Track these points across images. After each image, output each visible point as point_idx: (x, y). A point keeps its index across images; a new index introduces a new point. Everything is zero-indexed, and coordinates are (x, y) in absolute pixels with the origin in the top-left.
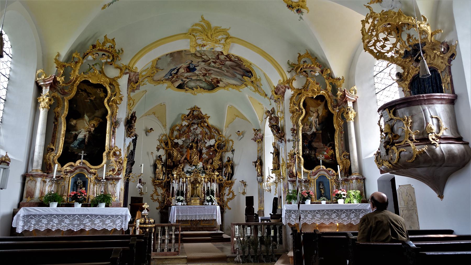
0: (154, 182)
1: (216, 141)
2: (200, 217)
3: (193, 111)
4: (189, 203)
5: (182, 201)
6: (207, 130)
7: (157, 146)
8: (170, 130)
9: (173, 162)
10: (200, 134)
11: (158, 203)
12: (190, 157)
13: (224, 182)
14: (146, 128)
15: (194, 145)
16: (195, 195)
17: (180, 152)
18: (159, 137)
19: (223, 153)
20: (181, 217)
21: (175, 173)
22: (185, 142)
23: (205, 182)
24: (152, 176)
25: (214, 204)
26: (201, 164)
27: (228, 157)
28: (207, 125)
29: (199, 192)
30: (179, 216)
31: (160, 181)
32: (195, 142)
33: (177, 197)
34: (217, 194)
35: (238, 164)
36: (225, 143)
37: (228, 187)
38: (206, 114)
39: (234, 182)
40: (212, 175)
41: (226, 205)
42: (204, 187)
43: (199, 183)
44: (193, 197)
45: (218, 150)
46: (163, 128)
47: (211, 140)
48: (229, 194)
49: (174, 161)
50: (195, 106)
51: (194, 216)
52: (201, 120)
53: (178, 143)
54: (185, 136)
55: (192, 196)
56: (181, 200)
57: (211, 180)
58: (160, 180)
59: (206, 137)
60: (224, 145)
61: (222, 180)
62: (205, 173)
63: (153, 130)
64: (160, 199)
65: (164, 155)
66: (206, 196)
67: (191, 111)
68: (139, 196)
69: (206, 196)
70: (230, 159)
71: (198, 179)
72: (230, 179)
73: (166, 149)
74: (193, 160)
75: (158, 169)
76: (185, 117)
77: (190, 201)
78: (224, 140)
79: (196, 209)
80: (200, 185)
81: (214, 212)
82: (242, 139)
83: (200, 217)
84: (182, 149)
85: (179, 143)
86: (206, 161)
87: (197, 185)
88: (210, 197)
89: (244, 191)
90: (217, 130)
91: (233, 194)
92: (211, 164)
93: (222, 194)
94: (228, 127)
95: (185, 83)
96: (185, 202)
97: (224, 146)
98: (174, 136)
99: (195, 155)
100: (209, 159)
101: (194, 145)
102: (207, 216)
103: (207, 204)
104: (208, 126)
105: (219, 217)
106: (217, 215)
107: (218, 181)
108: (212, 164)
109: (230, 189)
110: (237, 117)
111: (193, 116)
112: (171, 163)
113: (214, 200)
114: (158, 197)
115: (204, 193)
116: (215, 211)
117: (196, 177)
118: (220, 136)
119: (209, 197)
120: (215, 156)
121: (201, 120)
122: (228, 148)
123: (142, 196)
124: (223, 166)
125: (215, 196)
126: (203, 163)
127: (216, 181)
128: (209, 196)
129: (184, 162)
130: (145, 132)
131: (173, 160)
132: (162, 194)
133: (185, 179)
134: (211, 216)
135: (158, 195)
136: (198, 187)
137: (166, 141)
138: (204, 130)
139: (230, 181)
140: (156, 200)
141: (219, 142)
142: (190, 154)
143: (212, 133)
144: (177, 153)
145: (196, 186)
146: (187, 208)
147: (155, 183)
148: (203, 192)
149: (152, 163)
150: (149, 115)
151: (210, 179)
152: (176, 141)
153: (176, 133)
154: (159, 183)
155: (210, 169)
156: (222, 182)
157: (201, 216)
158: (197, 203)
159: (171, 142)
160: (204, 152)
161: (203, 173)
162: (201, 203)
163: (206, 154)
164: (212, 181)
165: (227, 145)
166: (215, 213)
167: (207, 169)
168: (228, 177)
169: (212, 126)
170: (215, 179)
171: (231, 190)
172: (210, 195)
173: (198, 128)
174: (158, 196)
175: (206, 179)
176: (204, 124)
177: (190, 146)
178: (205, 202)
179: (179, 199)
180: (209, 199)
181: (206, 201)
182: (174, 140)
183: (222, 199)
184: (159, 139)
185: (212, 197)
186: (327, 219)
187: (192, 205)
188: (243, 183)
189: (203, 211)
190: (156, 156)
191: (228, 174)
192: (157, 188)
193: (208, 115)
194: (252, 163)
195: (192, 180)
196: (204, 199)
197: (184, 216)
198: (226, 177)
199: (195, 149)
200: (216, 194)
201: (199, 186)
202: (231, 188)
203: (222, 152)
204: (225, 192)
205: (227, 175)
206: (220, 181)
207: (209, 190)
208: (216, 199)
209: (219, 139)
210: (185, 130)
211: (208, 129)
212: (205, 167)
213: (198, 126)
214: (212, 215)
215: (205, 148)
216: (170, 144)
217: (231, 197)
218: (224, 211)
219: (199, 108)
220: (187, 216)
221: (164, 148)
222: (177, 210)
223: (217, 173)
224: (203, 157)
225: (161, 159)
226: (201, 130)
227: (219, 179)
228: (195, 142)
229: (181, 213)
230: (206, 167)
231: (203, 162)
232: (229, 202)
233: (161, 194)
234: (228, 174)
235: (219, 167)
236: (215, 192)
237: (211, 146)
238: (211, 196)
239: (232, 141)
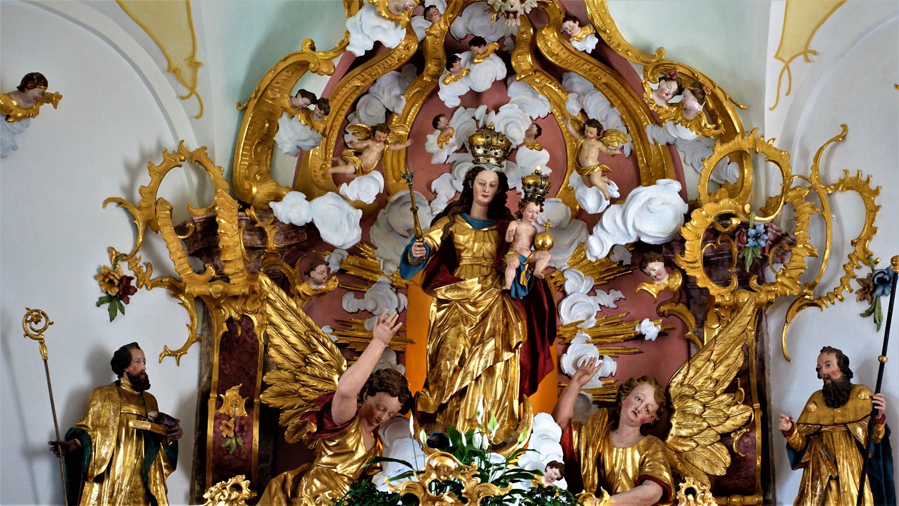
1: (694, 205)
7: (106, 262)
8: (243, 110)
12: (435, 359)
18: (133, 172)
19: (772, 323)
26: (545, 437)
27: (826, 350)
28: (591, 44)
32: (477, 211)
36: (793, 221)
45: (714, 289)
46: (168, 89)
47: (643, 194)
49: (277, 411)
54: (372, 157)
59: (591, 160)
60: (778, 240)
63: (53, 99)
65: (177, 355)
70: (848, 374)
75: (100, 479)
78: (775, 190)
84: (360, 295)
86: (601, 405)
92: (646, 429)
94: (807, 53)
95: (724, 282)
99: (483, 342)
100: (626, 387)
112: (243, 428)
118: (731, 146)
122: (817, 257)
124: (779, 444)
126: (568, 428)
129: (365, 415)
131: (266, 397)
137: (200, 214)
138: (573, 108)
141: (726, 204)
143: (651, 132)
144: (300, 327)
155: (640, 479)
160: (579, 314)
163: (599, 340)
169: (645, 52)
173: (514, 89)
176: (565, 36)
177: (431, 251)
182: (278, 198)
184: (129, 190)
186: (342, 480)
190: (93, 361)
199: (473, 285)
203: (760, 313)
209: (718, 186)
210: (389, 114)
212: (588, 465)
213: (511, 72)
215: (588, 284)
221: (176, 288)
224: (567, 363)
225: (141, 382)
226: (541, 108)
228: (477, 211)
230: (599, 463)
231: (567, 410)
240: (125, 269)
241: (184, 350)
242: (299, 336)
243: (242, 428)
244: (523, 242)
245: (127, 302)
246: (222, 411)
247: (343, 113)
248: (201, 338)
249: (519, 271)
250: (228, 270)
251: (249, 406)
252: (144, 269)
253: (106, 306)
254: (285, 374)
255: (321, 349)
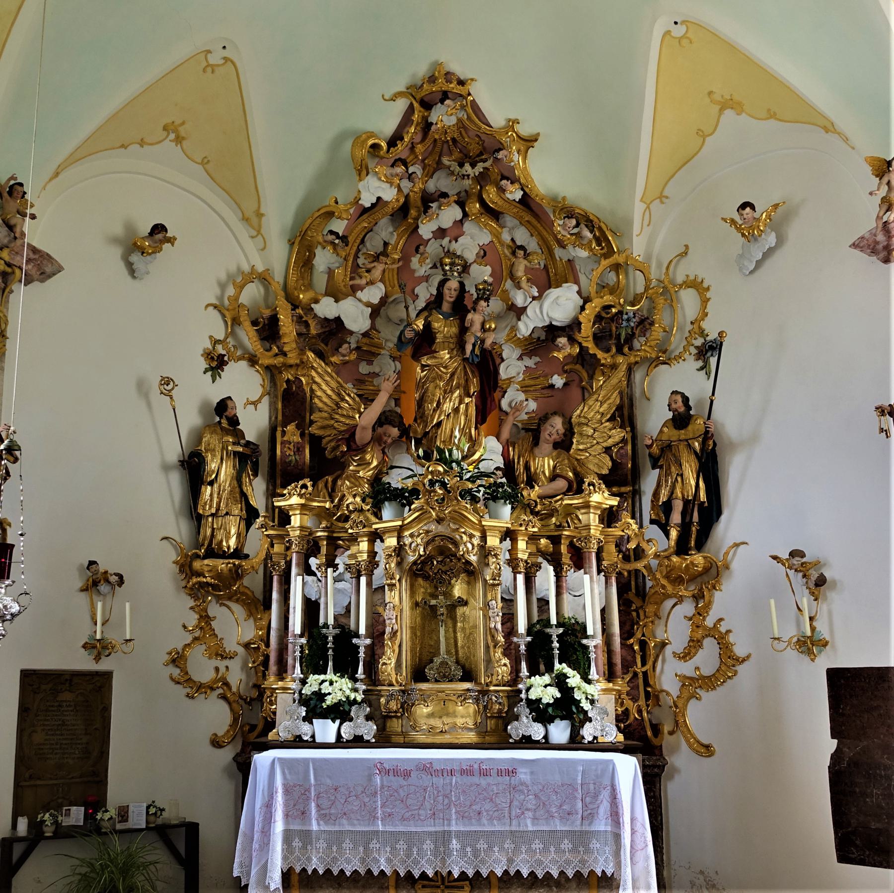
0: (186, 568)
1: (587, 300)
2: (476, 853)
3: (427, 105)
4: (395, 725)
5: (339, 712)
6: (522, 236)
8: (292, 244)
9: (315, 442)
10: (484, 254)
11: (224, 707)
12: (421, 403)
13: (654, 563)
14: (130, 228)
15: (444, 328)
16: (444, 664)
17: (360, 381)
18: (223, 286)
19: (638, 376)
20: (322, 845)
21: (295, 500)
22: (389, 320)
23: (513, 562)
24: (180, 530)
25: (588, 732)
26: (492, 451)
27: (675, 393)
28: (518, 195)
29: (474, 642)
30: (306, 836)
31: (222, 565)
32: (446, 307)
33: (303, 682)
34: (610, 652)
35: (754, 438)
36: (652, 309)
37: (681, 600)
38: (512, 124)
39: (727, 567)
40: (569, 512)
41: (678, 725)
42: (509, 603)
43: (471, 573)
44: (426, 680)
45: (600, 355)
47: (553, 293)
48: (695, 644)
49: (320, 438)
50: (437, 65)
51: (428, 845)
52: (480, 167)
53: (338, 320)
54: (377, 273)
55: (419, 675)
56: (329, 701)
57: (564, 549)
58: (224, 555)
59: (520, 272)
60: (642, 322)
61: (639, 554)
62: (514, 499)
63: (171, 241)
64: (236, 677)
66: (524, 671)
67: (411, 109)
68: (84, 663)
69: (524, 671)
70: (689, 408)
71: (456, 544)
72: (700, 547)
73: (267, 361)
74: (439, 424)
75: (211, 483)
76: (375, 147)
77: (406, 707)
78: (640, 289)
79: (439, 781)
80: (480, 585)
81: (589, 816)
82: (768, 263)
83: (476, 853)
84: (370, 363)
85: (349, 324)
86: (527, 430)
87: (458, 590)
88: (560, 682)
89: (813, 629)
90: (586, 220)
91: (725, 647)
92: (556, 445)
93: (643, 644)
94: (662, 198)
96: (368, 718)
97: (645, 323)
98: (320, 281)
100: (545, 418)
101: (444, 328)
102: (537, 845)
103: (537, 731)
104: (526, 201)
105: (639, 855)
106: (617, 837)
107: (612, 556)
108: (563, 445)
109: (701, 613)
110: (728, 113)
111: (429, 142)
112: (299, 450)
113: (586, 705)
114: (222, 664)
115: (510, 650)
116: (604, 808)
117: (440, 529)
119: (547, 679)
120: (585, 393)
121: (480, 167)
122: (668, 332)
123: (104, 665)
124: (643, 454)
125: (593, 674)
127: (599, 560)
128: (550, 669)
130: (117, 252)
131: (313, 430)
132: (247, 646)
133: (364, 545)
134: (566, 845)
135: (223, 656)
136: (463, 603)
137: (267, 313)
139: (698, 559)
140: (201, 688)
141: (608, 299)
142: (420, 384)
143: (558, 252)
144: (334, 384)
145: (448, 594)
146: (370, 778)
147: (200, 574)
148: (501, 638)
149: (174, 452)
150: (142, 143)
151: (555, 540)
152: (326, 308)
153: (323, 259)
154: (218, 576)
155: (554, 477)
156: (640, 565)
157: (482, 845)
158: (454, 726)
159: (299, 320)
160: (512, 372)
161: (495, 499)
162: (491, 724)
163: (525, 389)
164: (566, 559)
165: (662, 318)
166: (602, 825)
167: (531, 482)
168: (685, 528)
169: (554, 199)
170: (588, 538)
171: (709, 622)
172: (557, 666)
173: (467, 226)
174: (223, 657)
175: (522, 545)
176: (502, 190)
177: (417, 333)
178: (517, 718)
179: (320, 696)
180: (550, 695)
181: (523, 710)
182: (317, 301)
183: (646, 683)
184: (221, 298)
185: (574, 679)
187: (422, 738)
188: (804, 570)
189: (503, 801)
190: (204, 409)
191: (678, 506)
192: (214, 609)
193: (524, 130)
194: (875, 415)
195: (416, 549)
196: (514, 697)
197: (347, 845)
198: (667, 534)
199: (445, 355)
200: (603, 659)
201: (471, 593)
202: (708, 606)
203: (630, 370)
204: (660, 635)
205: (676, 517)
206: (626, 559)
207: (547, 623)
208: (606, 691)
209: (602, 287)
210: (386, 244)
211: (527, 225)
212: (520, 469)
213: (465, 215)
214: (581, 839)
215: (517, 352)
216: (288, 327)
217: (707, 671)
218: (662, 768)
219: (461, 83)
220: (374, 845)
221: (253, 361)
222: (287, 791)
223: (602, 498)
224: (504, 404)
225: (234, 421)
226: (485, 238)
227: (620, 543)
228: (446, 307)
229: (323, 817)
231: (506, 433)
232: (693, 701)
233: (241, 650)
234: (678, 506)
235: (616, 466)
236: (590, 643)
237: (552, 331)
238: (565, 669)
239: (696, 285)
240: (220, 350)
241: (259, 400)
242: (333, 390)
243: (298, 449)
244: (477, 326)
245: (223, 371)
246: (285, 439)
247: (356, 245)
248: (271, 391)
249: (474, 345)
250: (286, 349)
251: (302, 435)
252: (232, 349)
253: (210, 373)
254: (325, 415)
255: (347, 398)
